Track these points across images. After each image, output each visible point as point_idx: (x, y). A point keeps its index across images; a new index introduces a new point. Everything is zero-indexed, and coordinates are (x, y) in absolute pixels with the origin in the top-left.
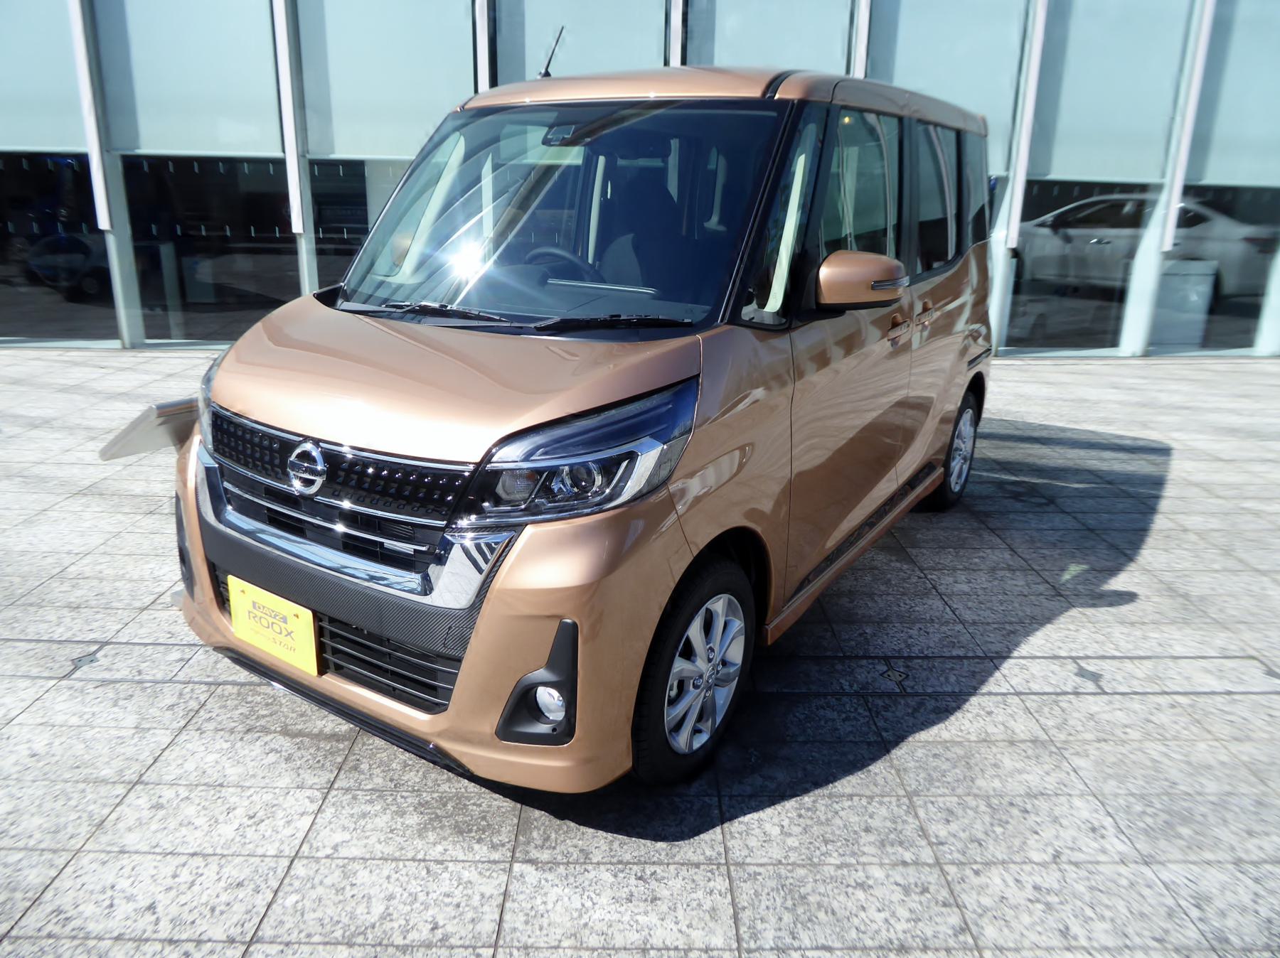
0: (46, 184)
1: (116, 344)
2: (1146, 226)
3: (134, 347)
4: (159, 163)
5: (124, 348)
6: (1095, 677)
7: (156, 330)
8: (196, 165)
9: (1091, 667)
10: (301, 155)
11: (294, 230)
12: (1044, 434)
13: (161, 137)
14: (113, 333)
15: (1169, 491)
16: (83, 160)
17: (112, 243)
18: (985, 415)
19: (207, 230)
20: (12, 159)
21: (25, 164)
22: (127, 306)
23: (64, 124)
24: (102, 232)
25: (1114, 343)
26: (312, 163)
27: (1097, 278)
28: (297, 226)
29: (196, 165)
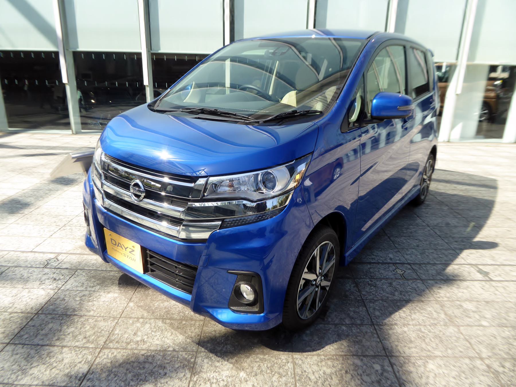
0: (43, 65)
1: (69, 132)
2: (450, 82)
3: (77, 133)
4: (88, 54)
5: (73, 134)
6: (486, 274)
7: (85, 125)
8: (22, 54)
9: (485, 269)
10: (148, 51)
11: (145, 84)
12: (449, 177)
13: (85, 45)
14: (67, 125)
15: (497, 208)
16: (139, 55)
17: (68, 88)
18: (437, 167)
19: (49, 83)
20: (6, 53)
21: (12, 55)
22: (74, 116)
23: (135, 43)
24: (64, 84)
25: (500, 136)
26: (153, 54)
27: (84, 126)
28: (146, 82)
29: (22, 54)
